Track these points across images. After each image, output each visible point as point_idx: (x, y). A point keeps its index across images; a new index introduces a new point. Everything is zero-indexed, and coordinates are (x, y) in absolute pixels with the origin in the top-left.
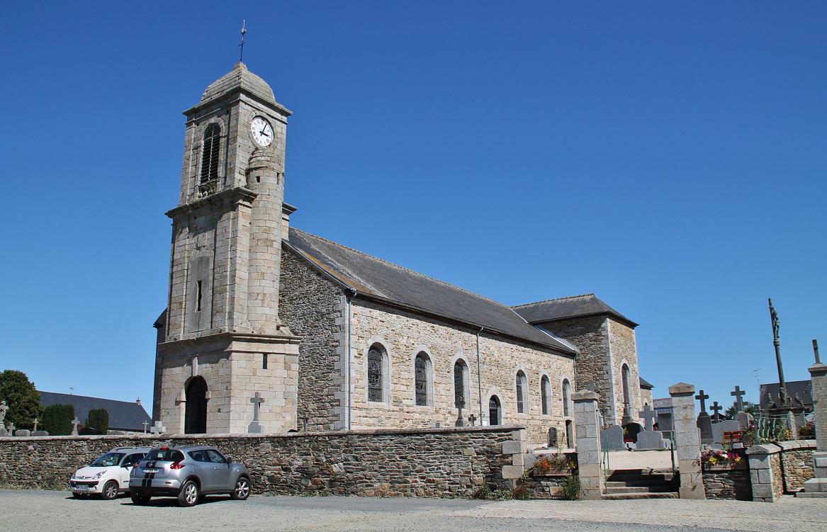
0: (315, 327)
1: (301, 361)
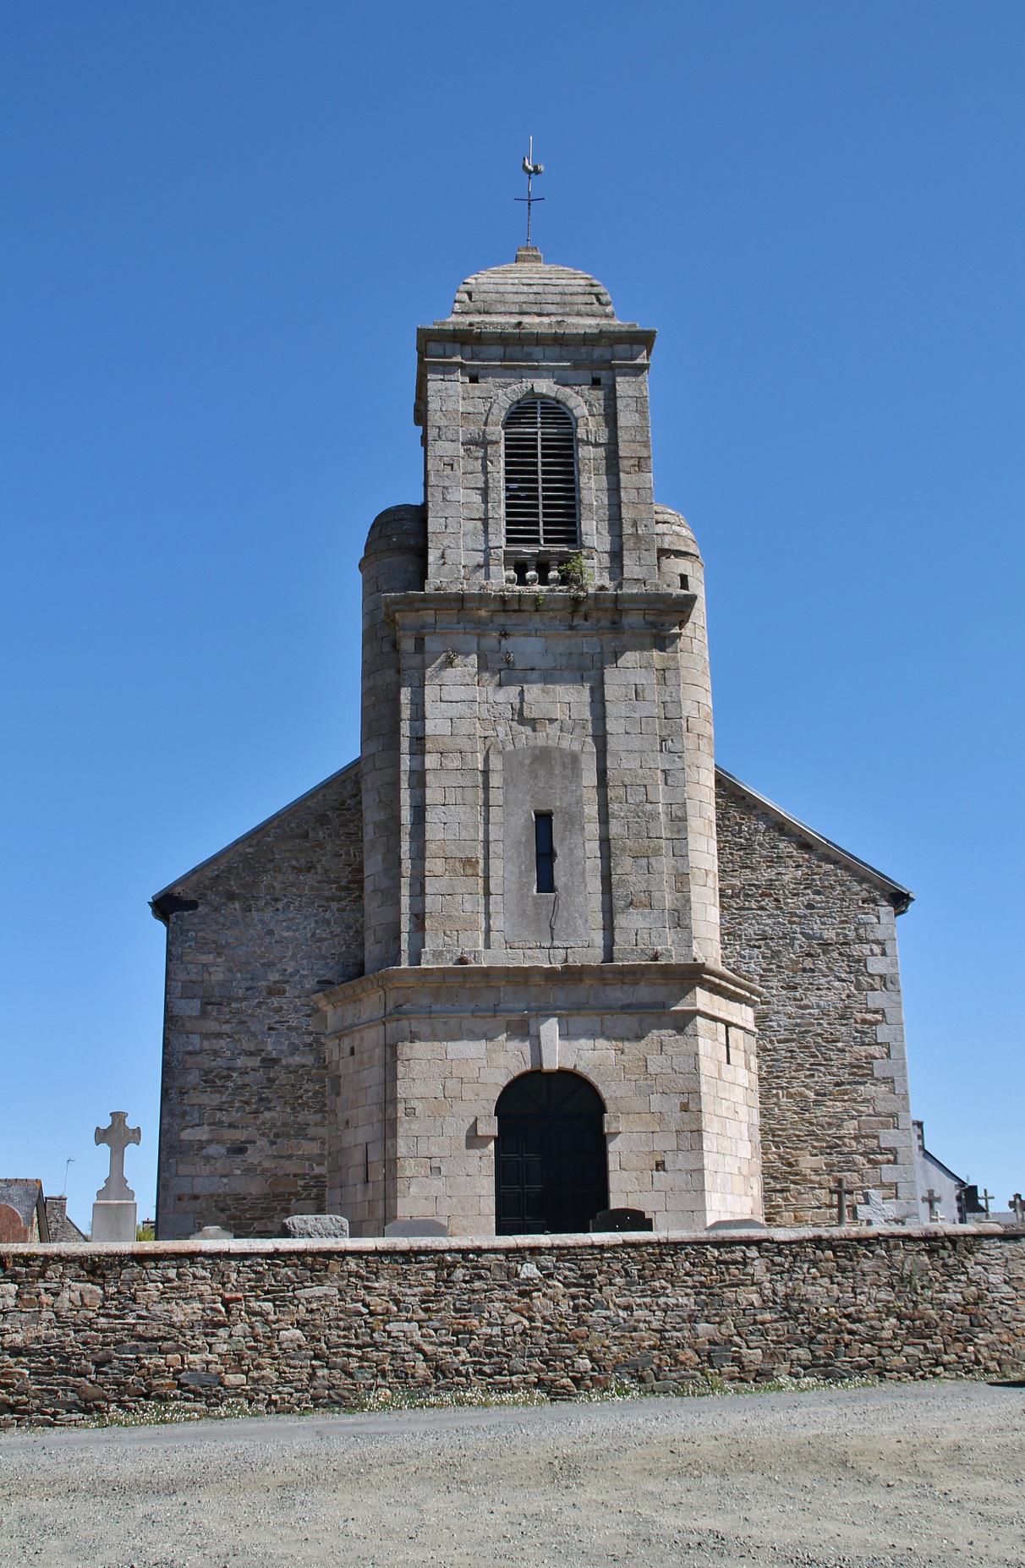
0: (804, 970)
1: (765, 1049)
